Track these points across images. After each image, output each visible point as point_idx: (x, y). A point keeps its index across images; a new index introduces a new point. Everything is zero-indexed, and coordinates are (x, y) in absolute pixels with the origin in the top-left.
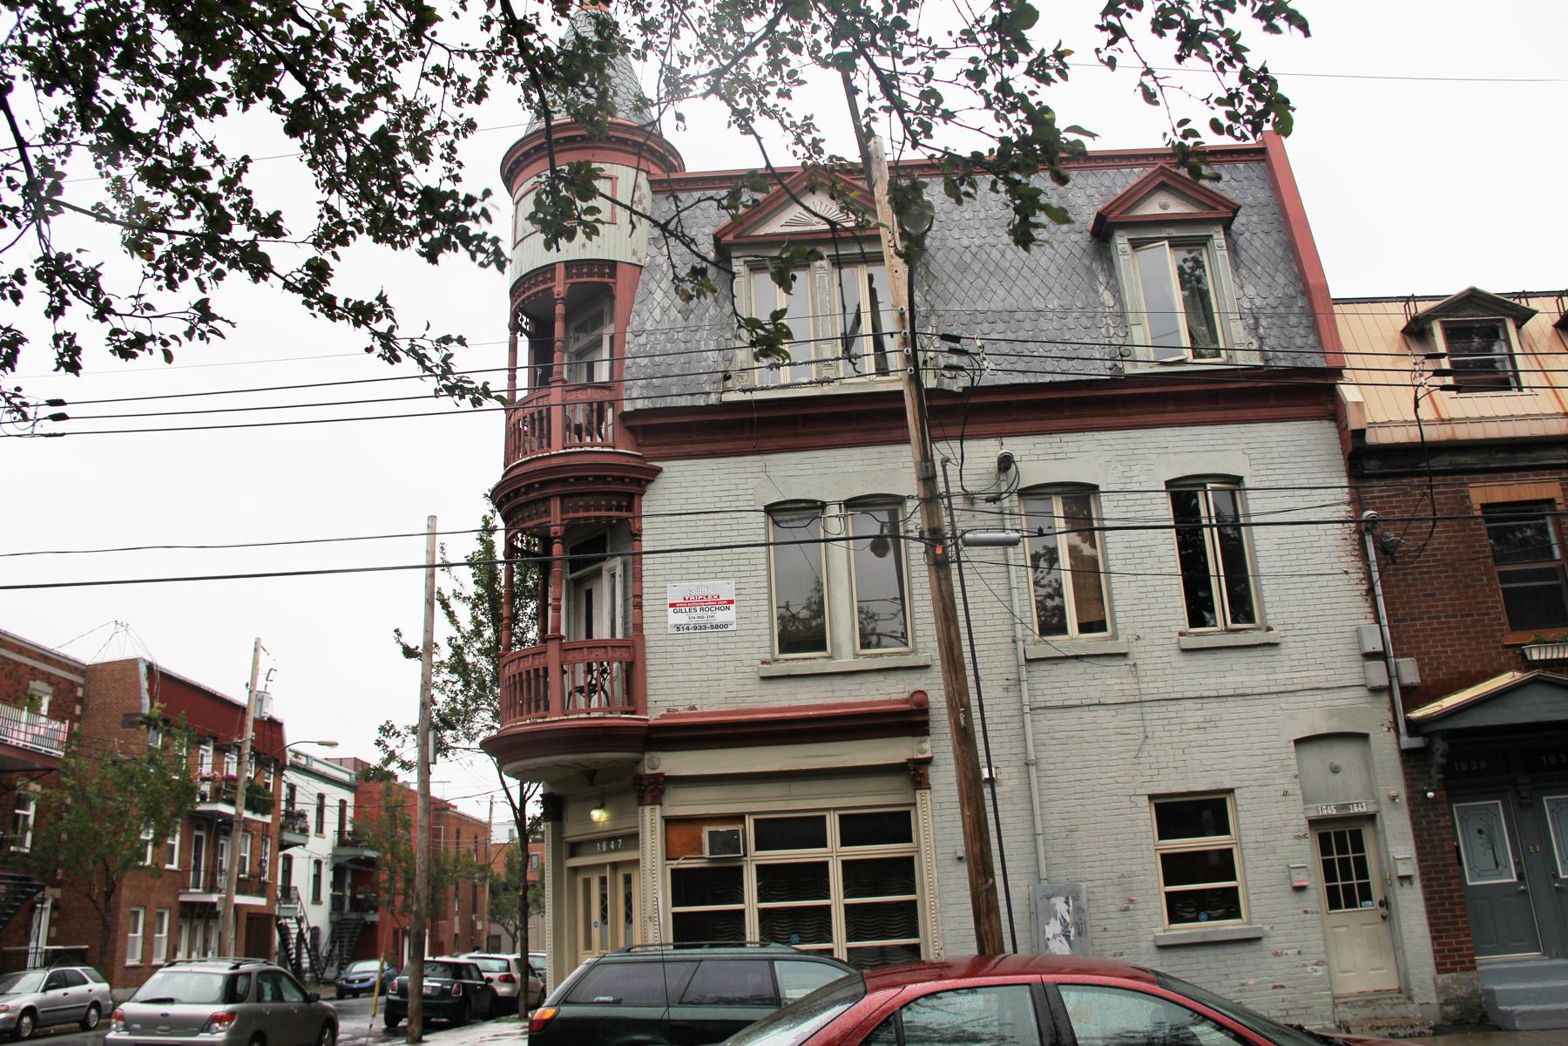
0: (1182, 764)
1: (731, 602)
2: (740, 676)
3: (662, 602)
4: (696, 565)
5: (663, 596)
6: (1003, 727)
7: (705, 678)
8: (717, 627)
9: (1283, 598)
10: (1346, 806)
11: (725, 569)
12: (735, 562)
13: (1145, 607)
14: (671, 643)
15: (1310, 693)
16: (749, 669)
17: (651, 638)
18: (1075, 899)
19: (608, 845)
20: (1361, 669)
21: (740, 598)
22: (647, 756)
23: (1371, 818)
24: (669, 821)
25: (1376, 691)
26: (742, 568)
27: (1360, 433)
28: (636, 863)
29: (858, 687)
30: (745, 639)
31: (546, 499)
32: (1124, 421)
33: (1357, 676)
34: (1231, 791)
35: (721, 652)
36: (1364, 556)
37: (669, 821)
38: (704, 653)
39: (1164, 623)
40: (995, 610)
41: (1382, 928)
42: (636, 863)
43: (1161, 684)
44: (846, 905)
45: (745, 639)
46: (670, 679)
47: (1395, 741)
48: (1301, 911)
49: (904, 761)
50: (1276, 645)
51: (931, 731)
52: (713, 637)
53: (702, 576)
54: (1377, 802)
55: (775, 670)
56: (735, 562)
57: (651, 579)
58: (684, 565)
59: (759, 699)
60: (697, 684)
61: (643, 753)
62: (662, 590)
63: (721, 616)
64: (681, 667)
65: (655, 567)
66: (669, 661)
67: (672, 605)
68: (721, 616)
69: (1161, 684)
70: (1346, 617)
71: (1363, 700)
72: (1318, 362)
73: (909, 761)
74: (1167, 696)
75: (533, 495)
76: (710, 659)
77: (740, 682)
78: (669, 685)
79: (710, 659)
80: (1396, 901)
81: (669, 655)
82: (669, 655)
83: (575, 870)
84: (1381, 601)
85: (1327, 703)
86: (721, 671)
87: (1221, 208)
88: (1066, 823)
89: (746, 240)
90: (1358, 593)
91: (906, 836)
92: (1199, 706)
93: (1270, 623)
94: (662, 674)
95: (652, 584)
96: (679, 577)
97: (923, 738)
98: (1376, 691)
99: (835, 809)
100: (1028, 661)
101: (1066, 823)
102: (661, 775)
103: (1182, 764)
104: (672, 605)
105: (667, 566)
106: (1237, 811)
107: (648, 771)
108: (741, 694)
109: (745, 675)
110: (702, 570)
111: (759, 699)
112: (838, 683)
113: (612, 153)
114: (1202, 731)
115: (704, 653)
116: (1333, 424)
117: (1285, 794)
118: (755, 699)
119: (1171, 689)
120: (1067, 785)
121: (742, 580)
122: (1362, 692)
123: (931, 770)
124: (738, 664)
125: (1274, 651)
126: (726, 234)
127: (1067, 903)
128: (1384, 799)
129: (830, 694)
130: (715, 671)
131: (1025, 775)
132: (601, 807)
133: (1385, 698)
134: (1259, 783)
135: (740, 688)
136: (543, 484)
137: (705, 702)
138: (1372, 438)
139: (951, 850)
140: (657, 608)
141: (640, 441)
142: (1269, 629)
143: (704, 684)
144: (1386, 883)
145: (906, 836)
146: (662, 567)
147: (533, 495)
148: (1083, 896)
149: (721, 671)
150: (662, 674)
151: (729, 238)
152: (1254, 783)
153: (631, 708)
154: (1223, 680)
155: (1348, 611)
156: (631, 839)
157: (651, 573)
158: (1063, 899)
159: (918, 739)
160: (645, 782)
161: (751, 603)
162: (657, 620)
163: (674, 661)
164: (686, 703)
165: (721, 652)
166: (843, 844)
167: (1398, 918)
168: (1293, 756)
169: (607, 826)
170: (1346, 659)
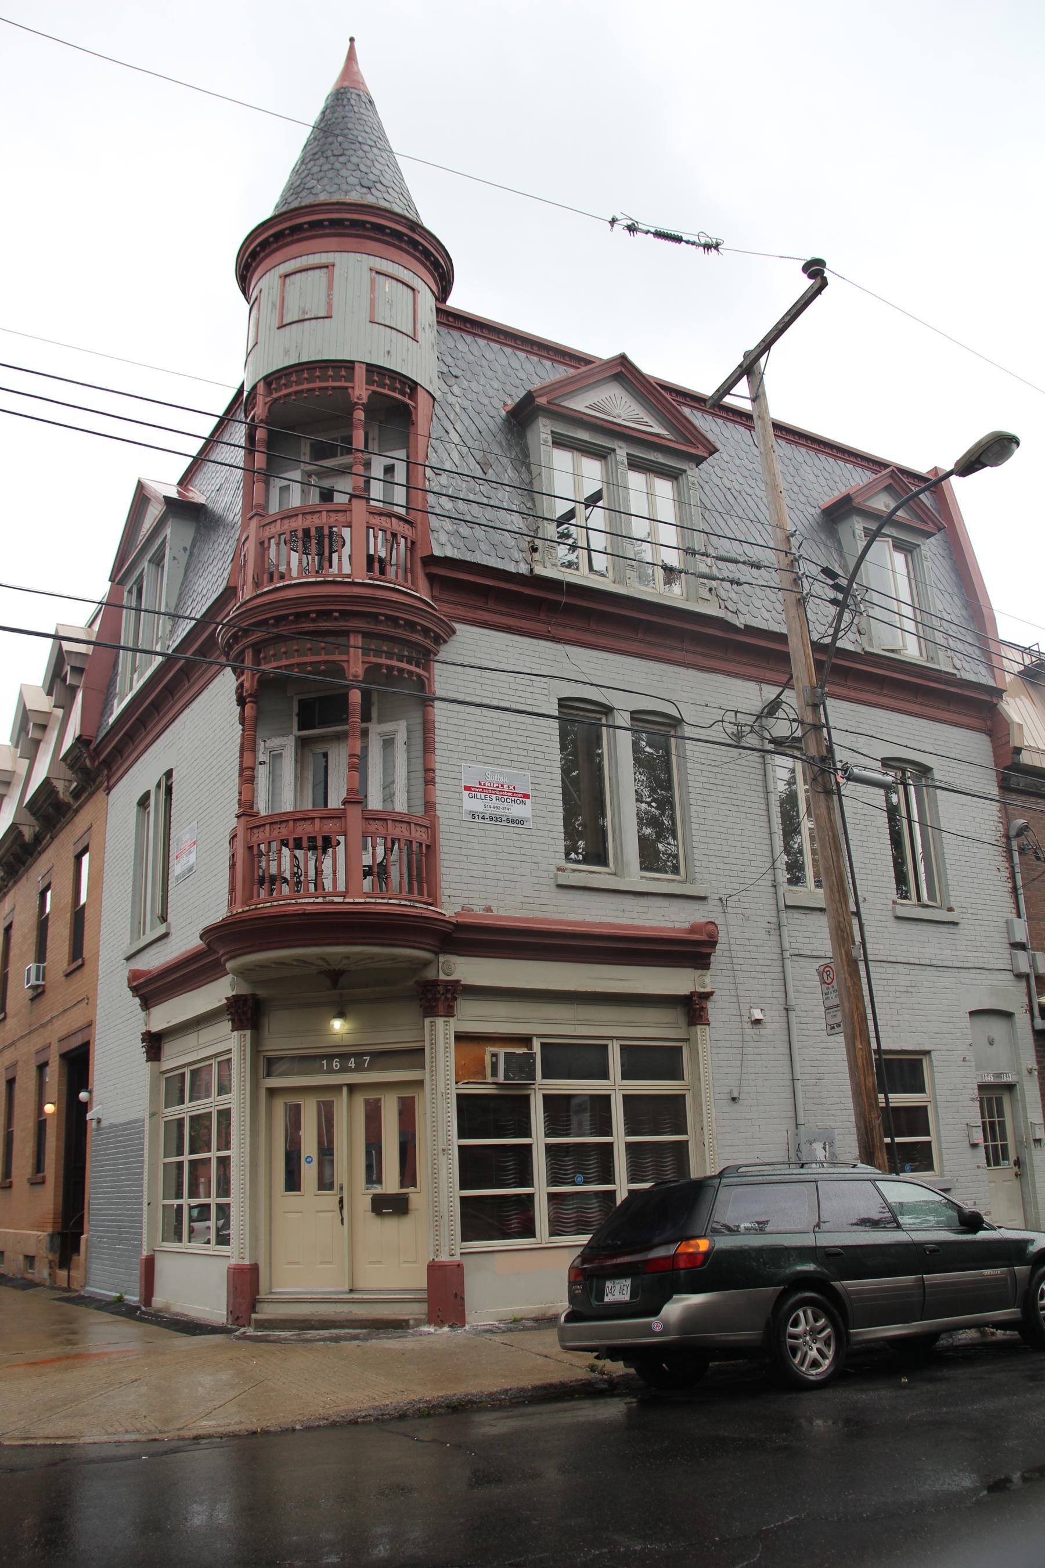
0: (896, 1023)
1: (527, 796)
2: (536, 880)
3: (456, 782)
4: (491, 748)
5: (457, 775)
6: (766, 969)
7: (501, 877)
8: (513, 821)
9: (961, 884)
10: (998, 1075)
11: (520, 758)
12: (530, 753)
13: (869, 872)
14: (466, 831)
15: (978, 971)
16: (545, 874)
17: (446, 822)
18: (831, 1146)
19: (330, 1064)
20: (1008, 956)
21: (536, 793)
22: (442, 958)
23: (1010, 1087)
24: (461, 1038)
25: (1019, 976)
26: (537, 761)
27: (1018, 751)
28: (420, 1083)
29: (645, 910)
30: (541, 840)
31: (346, 633)
32: (852, 694)
33: (1006, 961)
34: (928, 1053)
35: (517, 851)
36: (1010, 859)
37: (461, 1038)
38: (499, 849)
39: (882, 890)
40: (758, 852)
41: (1015, 1184)
42: (420, 1083)
43: (881, 947)
44: (547, 1145)
45: (541, 840)
46: (465, 873)
47: (1030, 1022)
48: (975, 1166)
49: (137, 1000)
50: (955, 924)
51: (711, 966)
52: (509, 831)
53: (497, 761)
54: (1019, 1073)
55: (564, 879)
56: (530, 753)
57: (445, 753)
58: (479, 746)
59: (554, 909)
60: (492, 883)
61: (437, 954)
62: (456, 769)
63: (518, 810)
64: (475, 860)
65: (448, 740)
66: (464, 852)
67: (467, 788)
68: (518, 810)
69: (881, 947)
70: (999, 909)
71: (1010, 983)
72: (988, 681)
73: (692, 994)
74: (885, 958)
75: (324, 625)
76: (506, 856)
77: (537, 887)
78: (464, 880)
79: (506, 856)
80: (1031, 1160)
81: (463, 845)
82: (463, 845)
83: (272, 1092)
84: (1022, 899)
85: (990, 982)
86: (517, 871)
87: (931, 524)
88: (815, 1070)
89: (555, 408)
90: (1006, 889)
91: (675, 1073)
92: (907, 971)
93: (953, 904)
94: (456, 865)
95: (445, 760)
96: (474, 758)
97: (705, 971)
98: (1019, 976)
99: (618, 1038)
100: (787, 907)
101: (815, 1070)
102: (458, 982)
103: (896, 1023)
104: (467, 788)
105: (461, 742)
106: (932, 1072)
107: (442, 977)
108: (537, 901)
109: (541, 881)
110: (497, 755)
111: (554, 909)
112: (629, 902)
113: (404, 255)
114: (909, 995)
115: (499, 849)
116: (988, 739)
117: (964, 1060)
118: (551, 908)
119: (888, 953)
120: (815, 1033)
121: (538, 774)
122: (1010, 976)
123: (710, 1005)
124: (534, 866)
125: (952, 929)
126: (540, 396)
127: (824, 1148)
128: (1025, 1072)
129: (620, 914)
130: (511, 871)
131: (784, 1019)
132: (341, 1015)
133: (1024, 984)
134: (948, 1047)
135: (536, 894)
136: (345, 615)
137: (501, 904)
138: (1026, 758)
139: (727, 1090)
140: (451, 788)
141: (436, 593)
142: (950, 909)
143: (501, 883)
144: (1020, 1144)
145: (675, 1073)
146: (455, 742)
147: (324, 625)
148: (837, 1143)
149: (517, 871)
150: (456, 865)
151: (542, 401)
152: (944, 1047)
153: (430, 900)
154: (921, 950)
155: (1001, 904)
156: (414, 1056)
157: (445, 746)
158: (822, 1145)
159: (699, 972)
160: (441, 989)
161: (546, 801)
162: (451, 802)
163: (469, 852)
164: (483, 902)
165: (517, 851)
166: (623, 1079)
167: (1033, 1176)
168: (968, 1025)
169: (349, 1040)
170: (1000, 945)
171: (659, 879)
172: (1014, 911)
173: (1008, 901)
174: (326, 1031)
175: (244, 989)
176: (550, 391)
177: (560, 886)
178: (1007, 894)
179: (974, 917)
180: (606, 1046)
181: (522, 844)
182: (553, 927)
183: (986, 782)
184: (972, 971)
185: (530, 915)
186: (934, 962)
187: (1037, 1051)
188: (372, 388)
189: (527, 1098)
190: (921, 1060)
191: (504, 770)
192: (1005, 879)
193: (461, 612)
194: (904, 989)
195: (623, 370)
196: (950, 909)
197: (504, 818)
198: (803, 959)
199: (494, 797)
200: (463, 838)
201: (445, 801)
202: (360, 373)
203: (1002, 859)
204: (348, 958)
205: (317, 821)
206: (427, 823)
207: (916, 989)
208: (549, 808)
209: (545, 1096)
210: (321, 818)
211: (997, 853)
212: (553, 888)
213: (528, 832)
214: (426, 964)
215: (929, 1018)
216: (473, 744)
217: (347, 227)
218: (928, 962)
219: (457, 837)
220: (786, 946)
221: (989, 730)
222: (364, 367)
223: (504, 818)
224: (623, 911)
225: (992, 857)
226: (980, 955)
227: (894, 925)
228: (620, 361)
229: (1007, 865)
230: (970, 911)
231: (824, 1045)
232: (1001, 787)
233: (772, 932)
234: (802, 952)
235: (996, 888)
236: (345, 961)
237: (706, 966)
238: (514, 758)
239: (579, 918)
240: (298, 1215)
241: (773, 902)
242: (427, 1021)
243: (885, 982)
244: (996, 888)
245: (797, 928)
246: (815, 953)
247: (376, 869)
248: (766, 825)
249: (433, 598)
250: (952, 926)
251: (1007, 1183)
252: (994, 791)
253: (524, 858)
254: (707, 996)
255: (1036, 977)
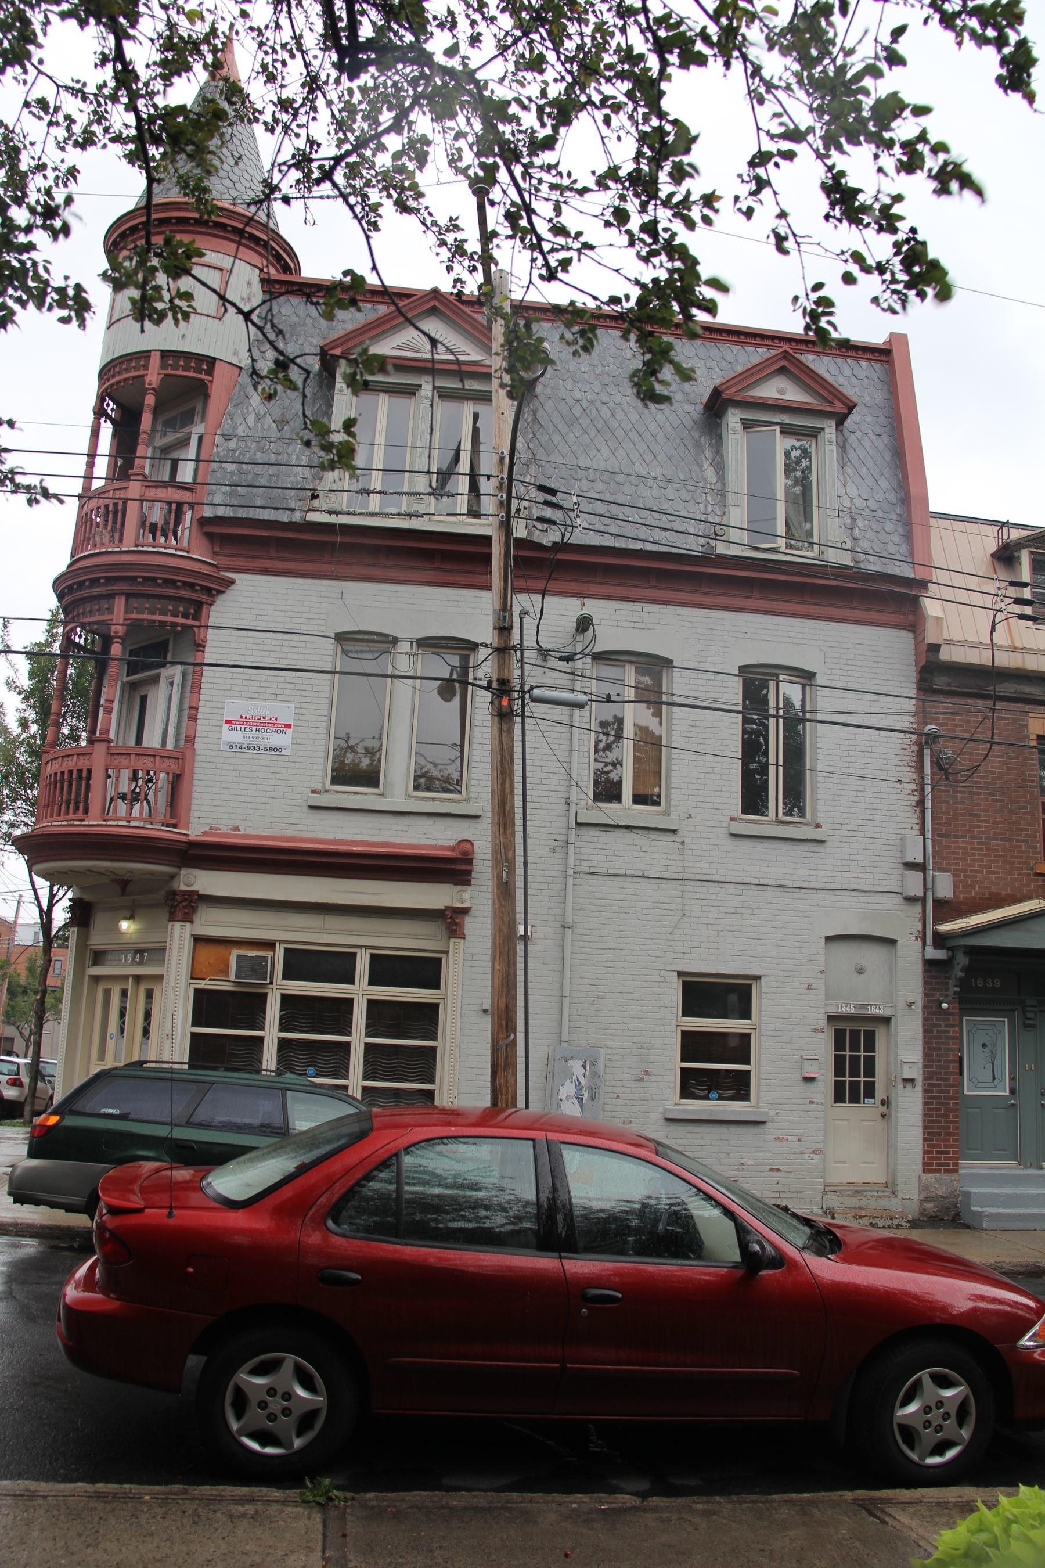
1: (289, 726)
6: (544, 886)
7: (253, 800)
8: (271, 749)
11: (286, 692)
12: (298, 687)
15: (848, 893)
18: (593, 1064)
21: (298, 723)
22: (184, 872)
23: (886, 1020)
24: (198, 940)
25: (910, 900)
26: (304, 693)
31: (111, 596)
32: (707, 600)
34: (758, 978)
36: (921, 769)
37: (198, 940)
40: (552, 770)
42: (160, 978)
47: (920, 950)
53: (262, 696)
54: (894, 1006)
56: (298, 687)
58: (245, 683)
62: (219, 705)
63: (277, 739)
67: (228, 722)
68: (277, 739)
69: (707, 865)
73: (447, 908)
74: (709, 878)
75: (97, 590)
78: (215, 803)
83: (96, 979)
84: (928, 814)
85: (862, 905)
86: (269, 794)
87: (837, 403)
90: (908, 803)
91: (434, 982)
93: (820, 821)
97: (465, 888)
99: (367, 947)
100: (578, 824)
104: (228, 722)
106: (761, 999)
107: (183, 887)
110: (263, 690)
114: (739, 916)
117: (809, 987)
121: (303, 705)
132: (131, 918)
133: (918, 908)
136: (109, 580)
138: (946, 654)
141: (217, 549)
142: (818, 826)
144: (891, 1084)
145: (434, 982)
147: (97, 590)
149: (269, 794)
153: (174, 822)
154: (766, 869)
156: (157, 953)
159: (459, 887)
166: (371, 983)
171: (433, 799)
172: (917, 827)
173: (913, 818)
174: (117, 929)
175: (78, 896)
176: (345, 342)
177: (311, 807)
178: (909, 809)
179: (852, 834)
180: (355, 954)
181: (278, 770)
182: (321, 846)
183: (898, 684)
184: (836, 892)
185: (278, 833)
186: (779, 883)
187: (925, 983)
188: (165, 372)
189: (265, 996)
190: (750, 986)
191: (268, 703)
192: (909, 792)
193: (241, 562)
194: (733, 910)
195: (437, 304)
196: (818, 826)
197: (262, 747)
198: (595, 877)
199: (254, 728)
200: (219, 766)
201: (205, 734)
202: (155, 360)
203: (909, 769)
204: (132, 872)
205: (133, 756)
206: (179, 755)
207: (749, 911)
208: (311, 736)
209: (283, 996)
210: (136, 754)
211: (901, 763)
212: (305, 809)
213: (287, 759)
214: (173, 877)
215: (762, 942)
216: (240, 682)
217: (192, 225)
218: (772, 882)
219: (213, 766)
220: (571, 863)
221: (910, 626)
222: (159, 353)
223: (262, 747)
224: (380, 830)
225: (893, 768)
226: (854, 875)
227: (730, 844)
228: (432, 295)
229: (915, 776)
230: (845, 827)
231: (611, 964)
232: (919, 689)
233: (558, 849)
234: (593, 870)
235: (893, 802)
236: (129, 875)
237: (468, 883)
238: (280, 692)
239: (329, 836)
240: (845, 1122)
241: (565, 819)
242: (171, 924)
243: (705, 903)
244: (893, 802)
245: (592, 845)
246: (610, 871)
247: (129, 797)
248: (567, 742)
249: (215, 554)
250: (815, 844)
251: (865, 1123)
252: (913, 693)
253: (278, 782)
254: (465, 911)
255: (934, 901)
